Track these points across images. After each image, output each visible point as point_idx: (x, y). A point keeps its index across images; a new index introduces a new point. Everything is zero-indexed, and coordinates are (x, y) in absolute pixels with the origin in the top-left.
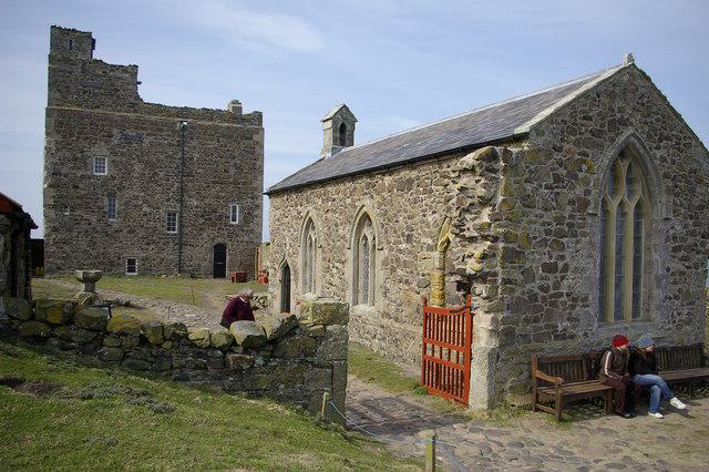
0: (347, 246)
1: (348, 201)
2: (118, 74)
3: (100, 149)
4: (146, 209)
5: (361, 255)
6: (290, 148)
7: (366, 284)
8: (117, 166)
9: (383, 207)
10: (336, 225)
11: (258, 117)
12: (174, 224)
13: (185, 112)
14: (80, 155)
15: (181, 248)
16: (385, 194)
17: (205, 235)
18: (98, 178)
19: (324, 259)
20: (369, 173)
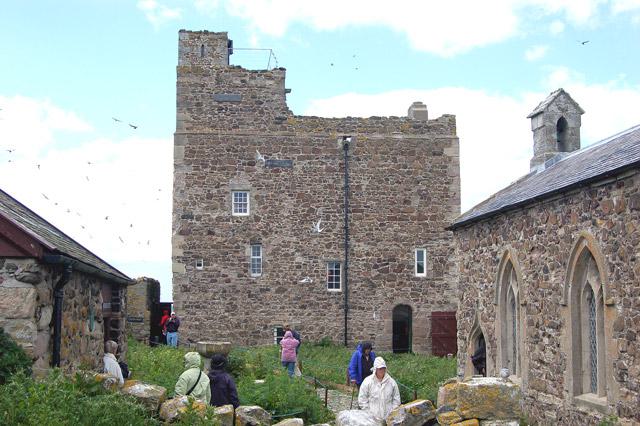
0: (562, 301)
1: (561, 232)
2: (260, 81)
3: (242, 181)
4: (299, 259)
5: (585, 316)
6: (493, 163)
7: (514, 335)
8: (260, 203)
9: (611, 238)
10: (546, 270)
11: (449, 122)
12: (338, 279)
13: (347, 124)
14: (215, 191)
15: (346, 312)
16: (614, 218)
17: (379, 294)
18: (418, 279)
19: (530, 323)
20: (587, 184)
